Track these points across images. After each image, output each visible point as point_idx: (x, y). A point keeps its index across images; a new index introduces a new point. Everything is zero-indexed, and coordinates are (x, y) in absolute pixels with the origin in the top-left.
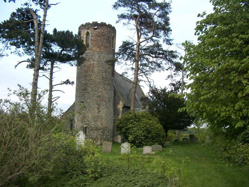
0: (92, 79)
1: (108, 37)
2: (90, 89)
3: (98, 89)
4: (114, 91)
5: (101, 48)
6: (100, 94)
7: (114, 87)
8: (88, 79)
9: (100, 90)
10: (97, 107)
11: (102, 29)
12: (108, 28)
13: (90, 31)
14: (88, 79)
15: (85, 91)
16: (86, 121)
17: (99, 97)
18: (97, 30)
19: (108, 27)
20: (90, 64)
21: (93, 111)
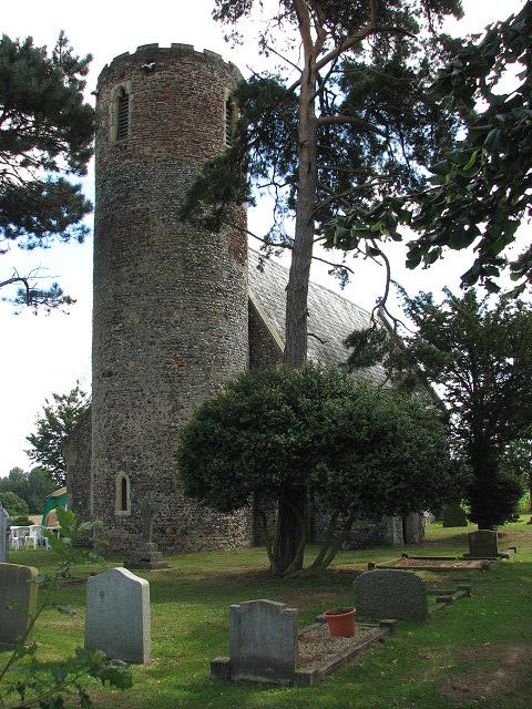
2: (133, 317)
3: (169, 314)
6: (177, 332)
8: (126, 275)
9: (177, 316)
15: (117, 328)
19: (203, 62)
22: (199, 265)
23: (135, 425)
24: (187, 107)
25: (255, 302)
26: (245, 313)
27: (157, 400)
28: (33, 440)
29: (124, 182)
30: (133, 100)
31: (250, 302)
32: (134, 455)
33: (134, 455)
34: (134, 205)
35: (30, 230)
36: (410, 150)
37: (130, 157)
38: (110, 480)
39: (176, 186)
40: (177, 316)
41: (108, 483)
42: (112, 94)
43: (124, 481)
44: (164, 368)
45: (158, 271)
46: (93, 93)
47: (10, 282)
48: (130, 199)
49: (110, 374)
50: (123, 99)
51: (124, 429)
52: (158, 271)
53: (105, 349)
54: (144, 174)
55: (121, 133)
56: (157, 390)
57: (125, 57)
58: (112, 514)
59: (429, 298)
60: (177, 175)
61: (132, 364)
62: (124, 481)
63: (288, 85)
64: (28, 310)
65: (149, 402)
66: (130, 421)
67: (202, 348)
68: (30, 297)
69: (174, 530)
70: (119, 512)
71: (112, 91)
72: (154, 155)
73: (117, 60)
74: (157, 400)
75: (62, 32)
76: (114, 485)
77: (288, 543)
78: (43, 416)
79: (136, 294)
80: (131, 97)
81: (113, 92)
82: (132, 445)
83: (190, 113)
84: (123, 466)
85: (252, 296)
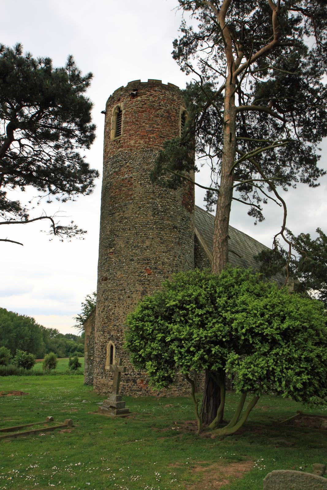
0: (127, 216)
1: (168, 112)
2: (121, 244)
3: (143, 242)
4: (196, 249)
5: (149, 138)
6: (148, 253)
7: (196, 240)
8: (117, 218)
9: (148, 243)
10: (141, 289)
11: (151, 95)
12: (167, 92)
13: (122, 103)
14: (117, 218)
15: (111, 251)
16: (111, 330)
17: (147, 260)
18: (139, 98)
19: (168, 90)
20: (123, 179)
21: (129, 301)
22: (162, 212)
23: (119, 311)
24: (157, 116)
25: (199, 237)
26: (192, 241)
27: (134, 296)
28: (81, 319)
29: (118, 162)
30: (125, 113)
31: (195, 236)
32: (118, 331)
33: (118, 331)
34: (123, 175)
35: (63, 190)
36: (299, 129)
37: (122, 147)
38: (103, 347)
39: (149, 163)
40: (148, 243)
41: (102, 349)
42: (113, 111)
43: (112, 347)
44: (139, 276)
45: (137, 215)
46: (103, 112)
47: (41, 218)
48: (122, 171)
49: (106, 279)
50: (119, 114)
51: (113, 314)
52: (137, 215)
53: (104, 264)
54: (130, 156)
55: (118, 133)
56: (134, 290)
57: (122, 89)
58: (104, 368)
59: (308, 236)
60: (150, 157)
61: (119, 273)
62: (112, 347)
63: (218, 87)
64: (57, 238)
65: (129, 297)
66: (117, 309)
67: (163, 264)
68: (57, 230)
69: (142, 381)
70: (108, 368)
71: (113, 110)
72: (137, 145)
73: (115, 91)
74: (134, 296)
75: (71, 57)
76: (106, 350)
77: (212, 401)
78: (86, 302)
79: (123, 229)
80: (123, 112)
81: (113, 110)
82: (118, 324)
83: (158, 119)
84: (111, 338)
85: (197, 233)
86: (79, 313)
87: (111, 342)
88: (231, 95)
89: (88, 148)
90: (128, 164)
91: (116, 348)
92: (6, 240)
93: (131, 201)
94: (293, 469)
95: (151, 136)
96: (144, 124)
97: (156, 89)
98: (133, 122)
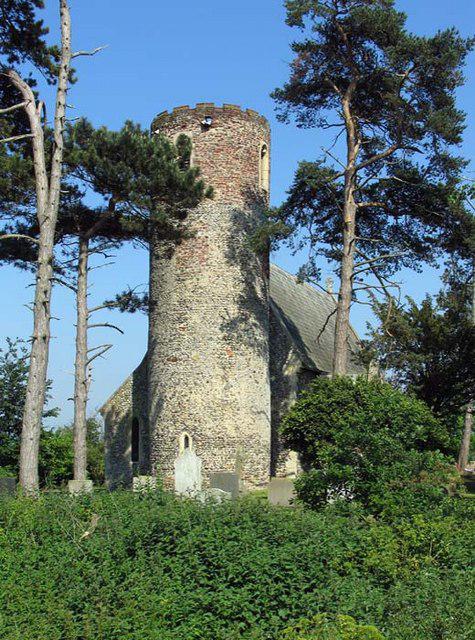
5: (228, 187)
12: (247, 124)
14: (190, 286)
27: (214, 380)
43: (187, 438)
74: (214, 380)
86: (460, 33)
87: (185, 433)
88: (148, 430)
89: (129, 124)
90: (201, 219)
91: (194, 439)
92: (106, 325)
93: (207, 268)
94: (15, 110)
95: (230, 184)
96: (221, 168)
97: (235, 119)
98: (206, 163)
